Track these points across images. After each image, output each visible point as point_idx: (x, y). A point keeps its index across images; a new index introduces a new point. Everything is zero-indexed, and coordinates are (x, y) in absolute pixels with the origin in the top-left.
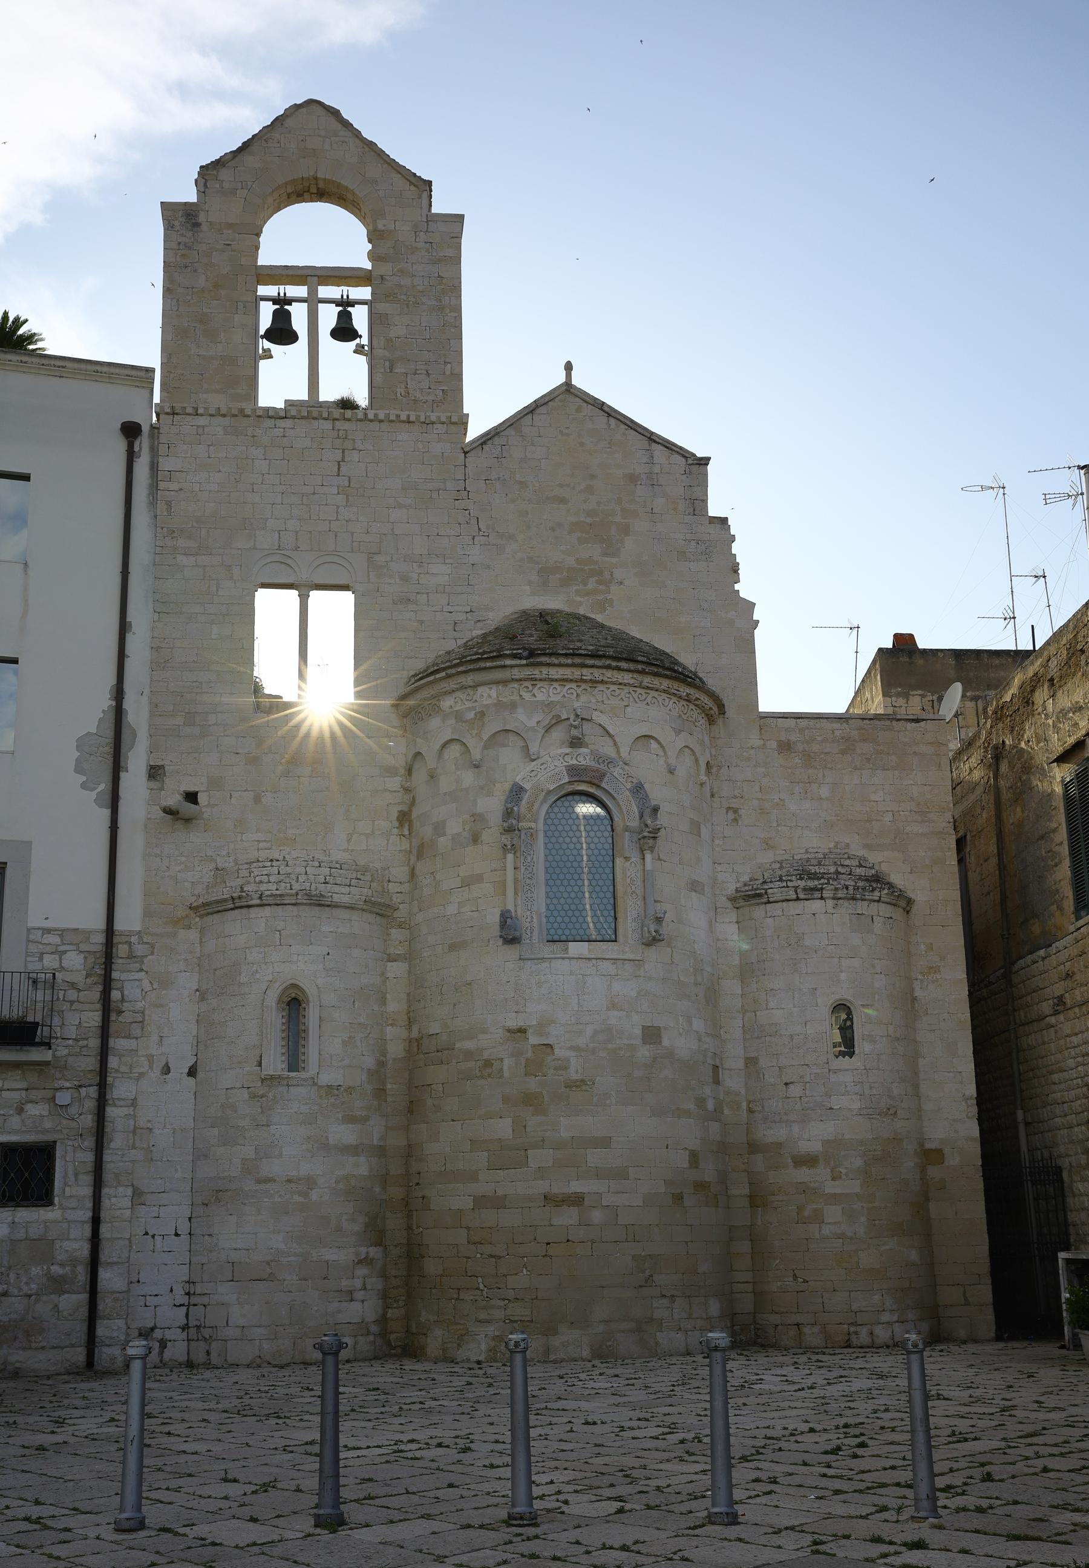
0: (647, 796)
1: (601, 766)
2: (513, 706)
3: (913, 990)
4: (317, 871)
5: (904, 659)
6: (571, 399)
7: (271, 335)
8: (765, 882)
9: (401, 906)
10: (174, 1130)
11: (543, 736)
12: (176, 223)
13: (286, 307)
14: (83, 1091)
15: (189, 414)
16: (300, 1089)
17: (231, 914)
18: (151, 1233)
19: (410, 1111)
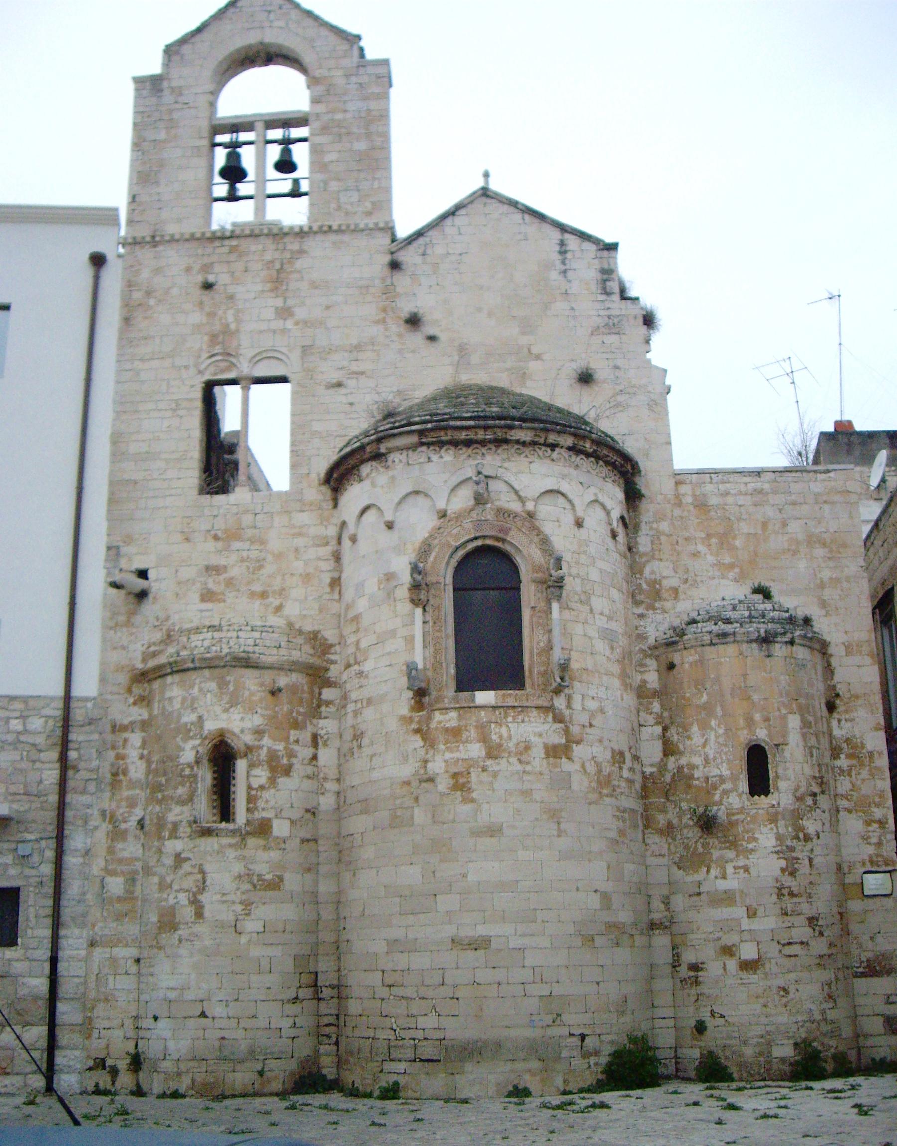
17: (169, 679)
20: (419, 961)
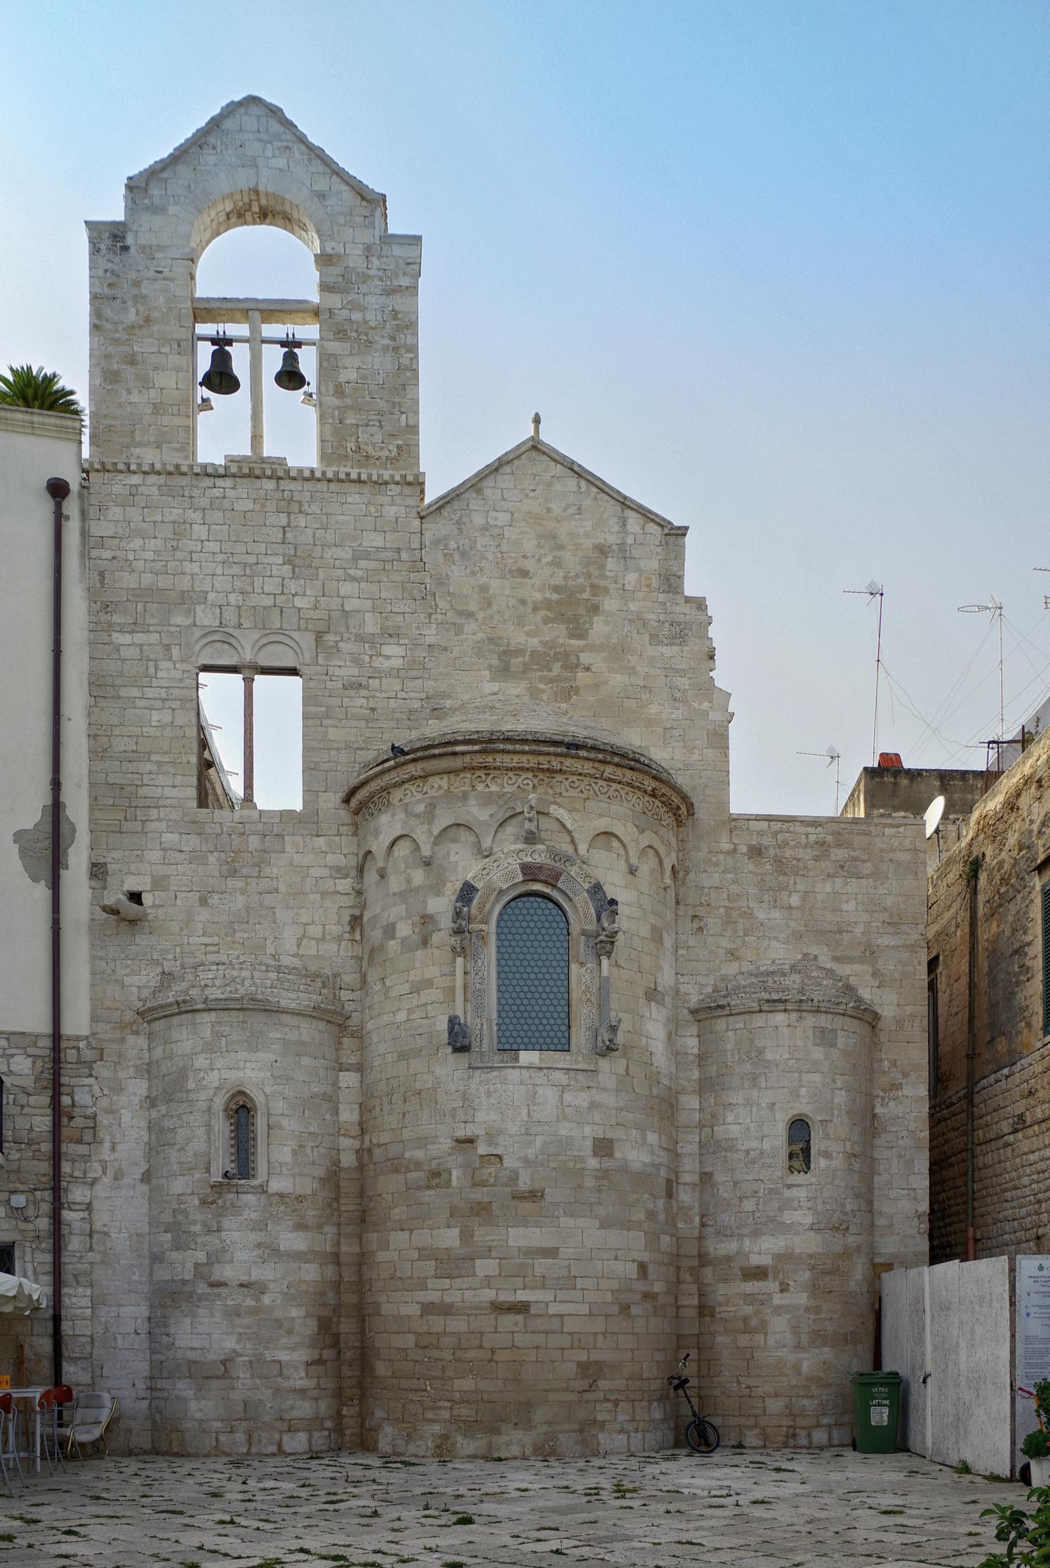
1: (558, 864)
3: (873, 1107)
7: (208, 381)
11: (496, 831)
12: (103, 247)
13: (227, 348)
14: (38, 1194)
15: (121, 472)
17: (176, 1020)
20: (458, 1325)
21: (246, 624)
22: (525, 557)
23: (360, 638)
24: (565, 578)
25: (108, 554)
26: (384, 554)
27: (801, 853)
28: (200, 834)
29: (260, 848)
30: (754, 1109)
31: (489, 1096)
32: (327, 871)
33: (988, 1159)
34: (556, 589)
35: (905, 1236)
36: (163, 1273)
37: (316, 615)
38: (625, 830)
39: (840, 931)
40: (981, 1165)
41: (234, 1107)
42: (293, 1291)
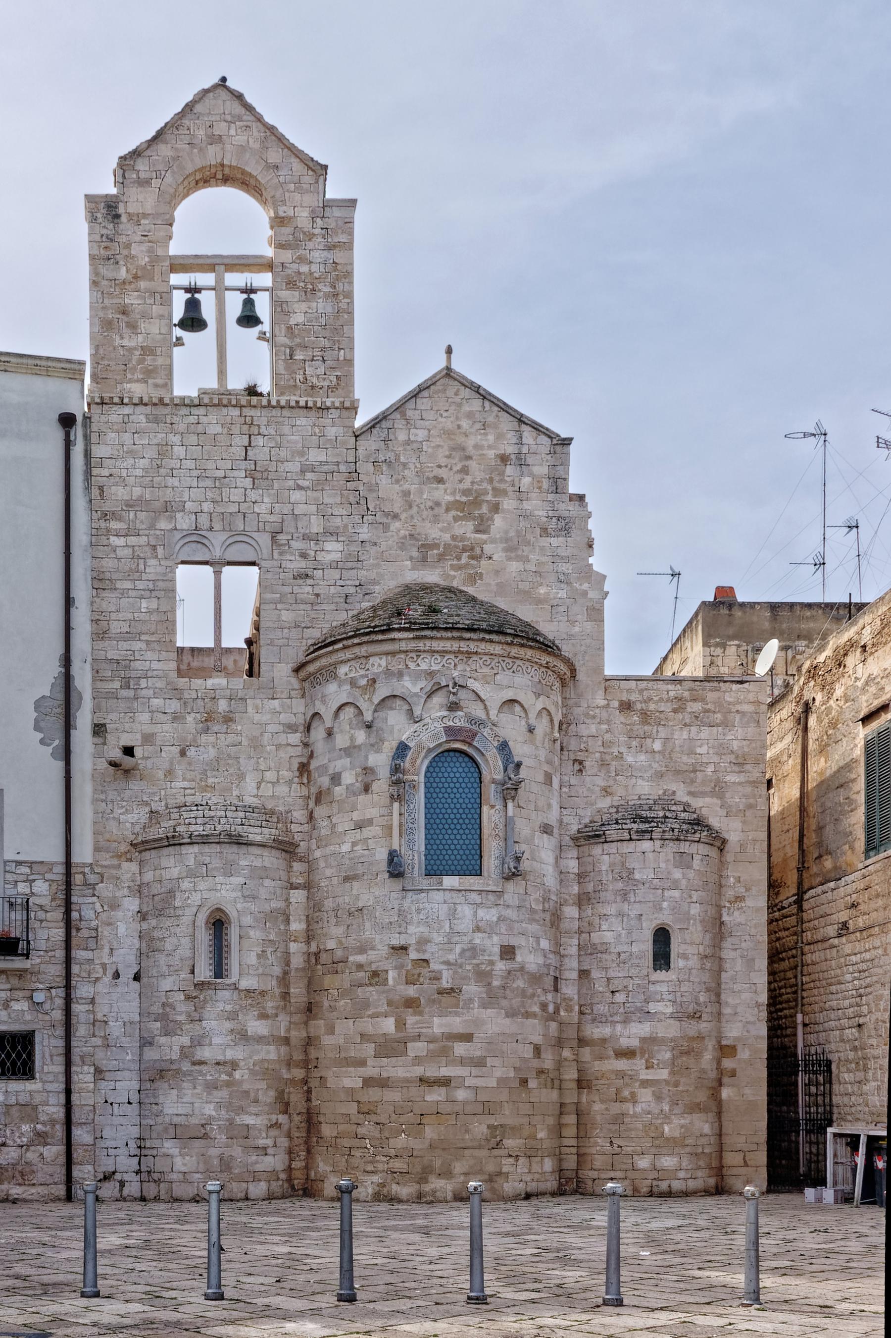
0: (511, 752)
2: (400, 674)
3: (721, 915)
4: (235, 814)
5: (724, 611)
6: (451, 382)
8: (603, 825)
9: (302, 843)
10: (125, 1023)
12: (99, 215)
14: (53, 991)
16: (225, 992)
17: (165, 851)
18: (109, 1102)
19: (309, 1010)
21: (217, 526)
22: (440, 467)
23: (306, 537)
24: (473, 483)
25: (106, 472)
26: (326, 467)
27: (663, 707)
28: (180, 699)
29: (227, 710)
30: (625, 919)
31: (419, 913)
32: (281, 728)
33: (816, 957)
34: (466, 492)
35: (747, 1022)
36: (151, 1054)
37: (272, 518)
38: (526, 698)
39: (695, 771)
40: (809, 962)
41: (212, 921)
42: (257, 1068)
